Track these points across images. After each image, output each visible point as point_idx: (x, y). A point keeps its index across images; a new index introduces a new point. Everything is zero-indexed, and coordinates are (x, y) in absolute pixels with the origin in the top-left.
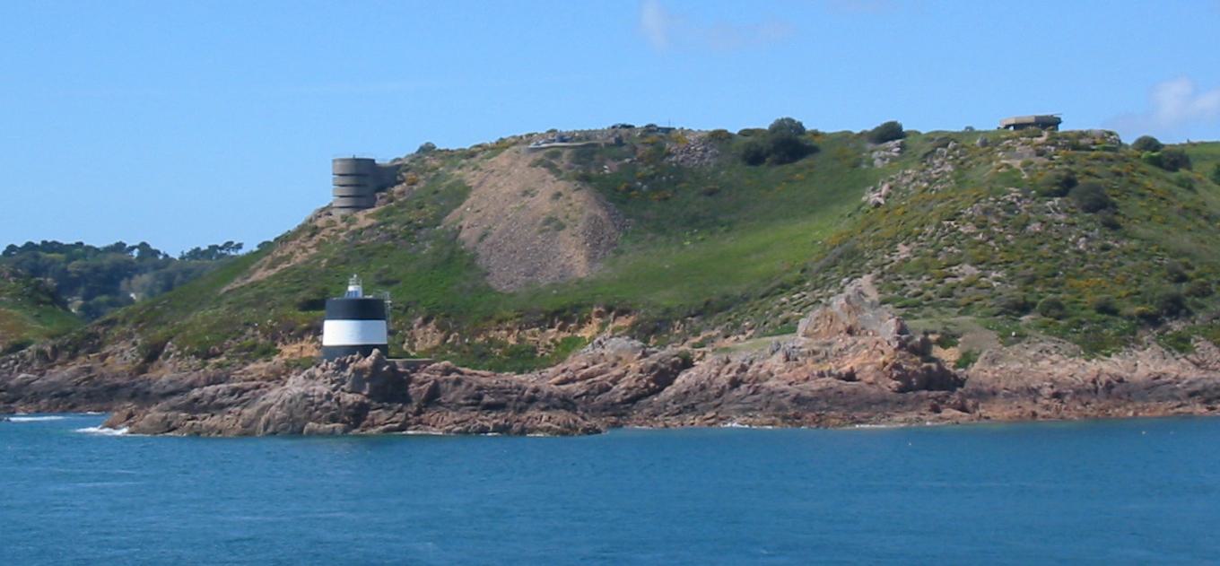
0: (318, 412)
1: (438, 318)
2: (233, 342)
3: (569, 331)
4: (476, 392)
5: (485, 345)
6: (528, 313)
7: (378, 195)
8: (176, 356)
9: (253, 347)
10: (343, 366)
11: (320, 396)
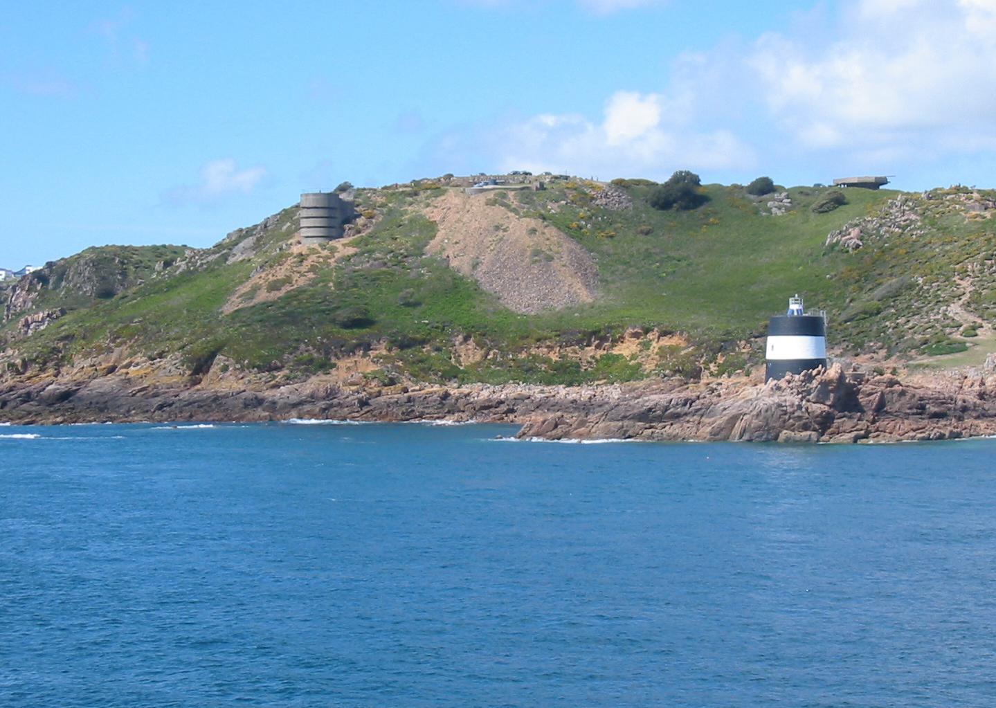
0: (791, 421)
1: (475, 337)
2: (291, 357)
3: (604, 350)
4: (919, 402)
5: (529, 361)
6: (564, 333)
7: (346, 226)
8: (235, 369)
9: (311, 361)
10: (810, 378)
11: (792, 406)
